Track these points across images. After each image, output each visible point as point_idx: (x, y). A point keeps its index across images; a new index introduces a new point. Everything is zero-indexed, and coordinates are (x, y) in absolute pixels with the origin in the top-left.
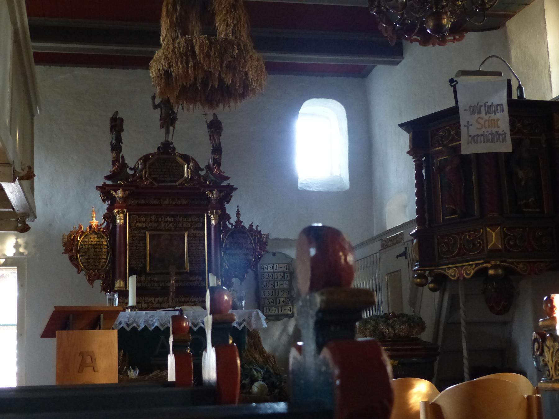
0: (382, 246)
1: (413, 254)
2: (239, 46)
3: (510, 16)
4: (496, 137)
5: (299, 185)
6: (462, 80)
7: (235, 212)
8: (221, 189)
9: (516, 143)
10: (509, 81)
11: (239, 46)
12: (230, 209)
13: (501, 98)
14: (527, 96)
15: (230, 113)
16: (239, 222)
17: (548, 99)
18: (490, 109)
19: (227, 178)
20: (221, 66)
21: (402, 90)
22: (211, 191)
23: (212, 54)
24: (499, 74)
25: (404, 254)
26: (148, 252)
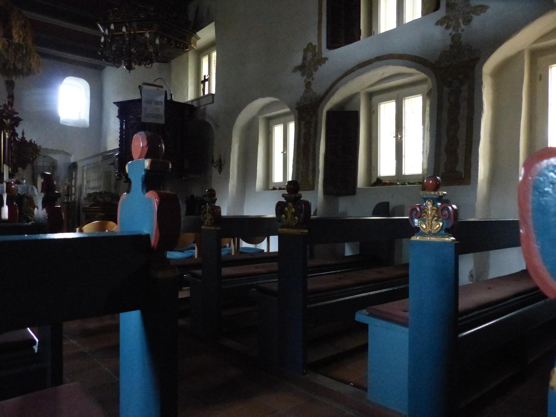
0: (103, 158)
1: (116, 164)
2: (26, 48)
3: (173, 59)
4: (157, 116)
5: (61, 122)
6: (145, 87)
7: (21, 133)
8: (13, 119)
9: (167, 120)
10: (166, 91)
11: (26, 48)
12: (18, 130)
13: (162, 98)
14: (175, 99)
15: (18, 81)
16: (23, 138)
17: (182, 102)
18: (157, 103)
19: (17, 113)
20: (15, 58)
21: (119, 83)
22: (7, 120)
23: (10, 50)
24: (162, 87)
25: (113, 164)
26: (319, 304)
